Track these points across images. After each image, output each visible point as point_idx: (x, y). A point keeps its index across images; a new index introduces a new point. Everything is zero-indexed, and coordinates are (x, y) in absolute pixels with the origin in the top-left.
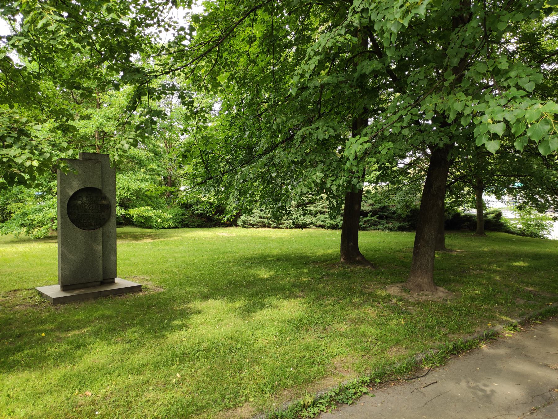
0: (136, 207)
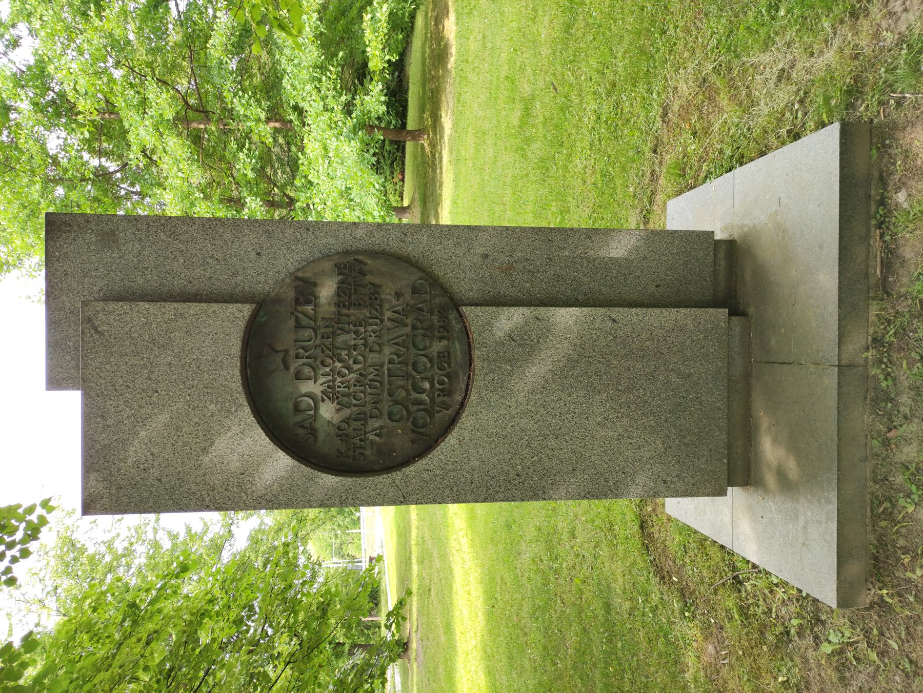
0: (364, 52)
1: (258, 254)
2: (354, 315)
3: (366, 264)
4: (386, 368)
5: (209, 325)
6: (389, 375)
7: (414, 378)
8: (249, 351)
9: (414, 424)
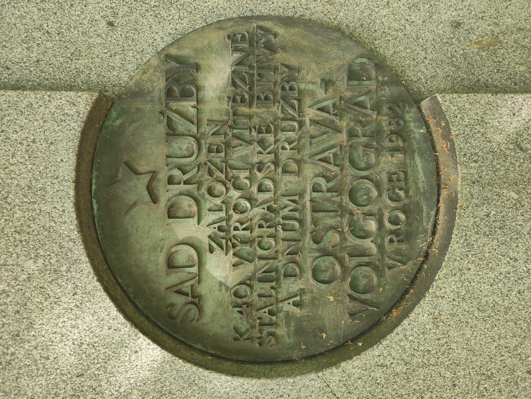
1: (111, 24)
2: (258, 115)
3: (275, 35)
4: (307, 198)
5: (22, 128)
6: (314, 210)
7: (352, 214)
8: (95, 173)
9: (353, 286)
